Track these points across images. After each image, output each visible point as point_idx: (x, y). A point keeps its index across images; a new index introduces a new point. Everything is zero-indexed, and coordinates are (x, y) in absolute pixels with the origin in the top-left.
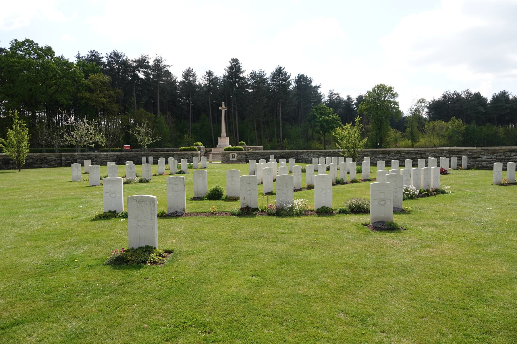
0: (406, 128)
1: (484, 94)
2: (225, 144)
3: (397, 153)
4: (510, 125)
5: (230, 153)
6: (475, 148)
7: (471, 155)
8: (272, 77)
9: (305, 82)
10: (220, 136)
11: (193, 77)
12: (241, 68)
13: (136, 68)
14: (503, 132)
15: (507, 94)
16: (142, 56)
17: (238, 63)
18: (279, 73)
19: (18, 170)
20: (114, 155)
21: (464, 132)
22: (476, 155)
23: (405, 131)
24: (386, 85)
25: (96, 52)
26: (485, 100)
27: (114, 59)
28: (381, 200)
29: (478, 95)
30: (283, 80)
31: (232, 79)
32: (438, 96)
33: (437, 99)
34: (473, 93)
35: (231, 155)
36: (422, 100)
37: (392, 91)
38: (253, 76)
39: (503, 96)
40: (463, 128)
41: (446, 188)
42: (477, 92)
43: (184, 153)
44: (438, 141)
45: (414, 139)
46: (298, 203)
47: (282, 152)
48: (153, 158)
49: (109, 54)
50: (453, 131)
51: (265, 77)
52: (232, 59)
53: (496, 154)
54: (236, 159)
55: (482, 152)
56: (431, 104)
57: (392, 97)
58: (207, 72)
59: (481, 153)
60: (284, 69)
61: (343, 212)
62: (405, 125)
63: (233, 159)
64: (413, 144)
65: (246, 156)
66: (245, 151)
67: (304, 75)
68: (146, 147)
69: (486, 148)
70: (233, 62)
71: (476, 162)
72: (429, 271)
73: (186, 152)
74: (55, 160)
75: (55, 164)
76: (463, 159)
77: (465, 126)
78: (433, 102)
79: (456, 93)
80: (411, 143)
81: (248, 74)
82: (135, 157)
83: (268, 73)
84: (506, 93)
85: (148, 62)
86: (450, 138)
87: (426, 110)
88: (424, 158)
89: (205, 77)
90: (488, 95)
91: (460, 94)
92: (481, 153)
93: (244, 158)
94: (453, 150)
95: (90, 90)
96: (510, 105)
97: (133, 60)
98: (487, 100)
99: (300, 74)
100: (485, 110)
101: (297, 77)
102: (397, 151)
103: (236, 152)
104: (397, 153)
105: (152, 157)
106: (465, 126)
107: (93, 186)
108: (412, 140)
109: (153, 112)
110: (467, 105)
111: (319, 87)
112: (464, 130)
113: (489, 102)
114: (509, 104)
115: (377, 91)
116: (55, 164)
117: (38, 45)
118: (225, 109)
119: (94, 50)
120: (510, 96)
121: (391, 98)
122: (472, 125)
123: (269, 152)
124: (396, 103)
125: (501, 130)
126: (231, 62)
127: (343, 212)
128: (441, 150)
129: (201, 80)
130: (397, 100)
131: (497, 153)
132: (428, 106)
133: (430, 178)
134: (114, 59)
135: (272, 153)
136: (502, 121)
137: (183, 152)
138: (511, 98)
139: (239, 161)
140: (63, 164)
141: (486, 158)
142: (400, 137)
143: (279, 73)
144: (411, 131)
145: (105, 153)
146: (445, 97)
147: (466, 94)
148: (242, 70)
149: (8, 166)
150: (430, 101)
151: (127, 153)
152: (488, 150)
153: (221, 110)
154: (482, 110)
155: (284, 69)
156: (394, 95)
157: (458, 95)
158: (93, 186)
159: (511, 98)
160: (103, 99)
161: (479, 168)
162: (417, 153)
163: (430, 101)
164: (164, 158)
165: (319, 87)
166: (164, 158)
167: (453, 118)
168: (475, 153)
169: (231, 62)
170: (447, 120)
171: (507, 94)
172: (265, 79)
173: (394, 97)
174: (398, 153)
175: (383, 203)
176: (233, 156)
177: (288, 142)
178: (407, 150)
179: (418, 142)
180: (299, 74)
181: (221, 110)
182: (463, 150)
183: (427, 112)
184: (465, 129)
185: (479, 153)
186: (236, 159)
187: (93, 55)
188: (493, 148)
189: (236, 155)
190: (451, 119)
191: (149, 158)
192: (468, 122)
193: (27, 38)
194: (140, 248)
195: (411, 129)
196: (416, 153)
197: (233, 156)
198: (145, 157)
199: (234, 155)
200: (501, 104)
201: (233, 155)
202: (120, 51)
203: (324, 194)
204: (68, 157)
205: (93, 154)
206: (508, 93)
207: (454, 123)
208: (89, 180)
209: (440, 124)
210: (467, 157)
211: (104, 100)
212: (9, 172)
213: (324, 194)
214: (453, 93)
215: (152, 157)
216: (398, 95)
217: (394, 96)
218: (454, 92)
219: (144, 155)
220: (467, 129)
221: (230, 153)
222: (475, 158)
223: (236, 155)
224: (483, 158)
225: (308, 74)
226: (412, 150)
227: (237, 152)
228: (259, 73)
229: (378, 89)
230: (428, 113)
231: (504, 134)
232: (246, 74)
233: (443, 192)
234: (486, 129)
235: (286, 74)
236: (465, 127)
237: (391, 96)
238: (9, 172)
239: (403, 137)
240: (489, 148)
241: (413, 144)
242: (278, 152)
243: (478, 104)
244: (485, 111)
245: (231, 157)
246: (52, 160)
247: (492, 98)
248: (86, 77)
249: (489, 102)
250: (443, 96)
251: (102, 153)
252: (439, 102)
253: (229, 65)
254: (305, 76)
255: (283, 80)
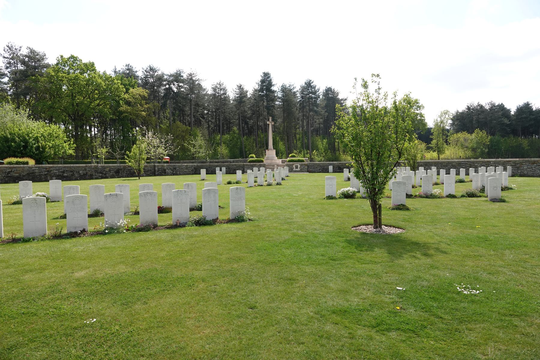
0: (432, 139)
1: (507, 106)
2: (272, 156)
3: (448, 164)
4: (534, 137)
5: (293, 164)
6: (518, 159)
7: (515, 166)
8: (301, 90)
9: (332, 95)
10: (267, 148)
11: (224, 90)
12: (272, 81)
13: (172, 82)
14: (527, 143)
15: (530, 105)
16: (177, 71)
17: (269, 77)
18: (309, 85)
19: (138, 178)
20: (192, 166)
21: (488, 143)
22: (518, 165)
23: (431, 143)
24: (412, 97)
25: (131, 66)
26: (509, 111)
27: (149, 73)
28: (494, 187)
29: (501, 107)
30: (312, 93)
31: (263, 93)
32: (462, 108)
33: (460, 111)
34: (497, 104)
35: (294, 166)
36: (445, 112)
37: (418, 103)
38: (284, 89)
39: (526, 107)
40: (488, 140)
41: (513, 186)
42: (500, 104)
43: (253, 165)
44: (463, 152)
45: (440, 151)
46: (436, 191)
47: (340, 164)
48: (226, 169)
49: (145, 69)
50: (477, 143)
51: (295, 90)
52: (263, 73)
53: (535, 165)
54: (299, 169)
55: (524, 162)
56: (454, 115)
57: (418, 109)
58: (237, 86)
59: (523, 164)
60: (313, 82)
61: (463, 196)
62: (431, 137)
63: (297, 169)
64: (439, 156)
65: (308, 167)
66: (307, 163)
67: (332, 88)
68: (208, 159)
69: (527, 159)
70: (264, 76)
71: (519, 171)
72: (433, 298)
73: (254, 163)
74: (150, 170)
75: (150, 174)
76: (508, 168)
77: (489, 137)
78: (457, 113)
79: (479, 105)
80: (437, 155)
81: (279, 88)
82: (209, 168)
83: (297, 85)
84: (530, 104)
85: (182, 77)
86: (474, 150)
87: (450, 122)
88: (455, 169)
89: (236, 90)
90: (512, 107)
91: (484, 105)
92: (523, 164)
93: (306, 168)
94: (499, 161)
95: (128, 103)
96: (534, 117)
97: (168, 75)
98: (511, 111)
99: (328, 87)
100: (509, 121)
101: (324, 90)
102: (449, 162)
103: (299, 163)
104: (448, 164)
105: (225, 168)
106: (489, 137)
107: (250, 187)
108: (438, 152)
109: (488, 148)
110: (491, 117)
111: (346, 100)
112: (489, 142)
113: (512, 113)
114: (533, 115)
115: (403, 103)
116: (150, 174)
117: (81, 61)
118: (272, 124)
119: (129, 64)
120: (533, 107)
121: (417, 110)
122: (497, 137)
123: (328, 163)
124: (422, 116)
125: (524, 142)
126: (262, 76)
127: (463, 196)
128: (488, 161)
129: (232, 94)
130: (423, 112)
131: (536, 164)
132: (452, 117)
133: (502, 179)
134: (149, 73)
135: (331, 164)
136: (527, 132)
137: (252, 163)
138: (534, 109)
139: (301, 171)
140: (157, 173)
141: (527, 168)
142: (425, 148)
143: (309, 85)
144: (437, 143)
145: (186, 164)
146: (469, 108)
147: (490, 105)
148: (273, 83)
149: (118, 175)
150: (454, 113)
151: (203, 164)
152: (529, 161)
153: (269, 124)
154: (506, 121)
155: (313, 82)
156: (420, 106)
157: (482, 107)
158: (250, 187)
159: (534, 109)
160: (143, 113)
161: (521, 176)
162: (467, 164)
163: (454, 113)
164: (205, 169)
165: (346, 100)
166: (205, 169)
167: (477, 129)
168: (518, 163)
169: (262, 76)
170: (471, 132)
171: (530, 105)
172: (295, 93)
173: (420, 110)
174: (450, 164)
175: (495, 189)
176: (297, 167)
177: (317, 155)
178: (457, 162)
179: (444, 153)
180: (326, 87)
181: (269, 124)
182: (507, 161)
183: (451, 124)
184: (489, 140)
185: (521, 163)
186: (299, 169)
187: (128, 69)
188: (533, 159)
189: (299, 166)
190: (475, 130)
191: (223, 168)
192: (493, 134)
193: (72, 54)
194: (402, 204)
195: (437, 141)
196: (465, 164)
197: (297, 167)
198: (219, 168)
199: (297, 166)
200: (525, 116)
201: (296, 166)
202: (155, 66)
203: (450, 186)
204: (160, 167)
205: (177, 165)
206: (531, 104)
207: (478, 135)
208: (247, 182)
209: (462, 136)
210: (511, 167)
211: (144, 113)
212: (131, 180)
213: (450, 186)
214: (477, 104)
215: (225, 168)
216: (424, 107)
217: (420, 108)
218: (478, 103)
219: (217, 166)
220: (491, 141)
221: (293, 164)
222: (518, 168)
223: (299, 166)
224: (525, 168)
225: (336, 87)
226: (462, 161)
227: (300, 163)
228: (289, 86)
229: (404, 102)
230: (452, 125)
231: (528, 146)
232: (277, 88)
233: (511, 189)
234: (512, 141)
235: (315, 87)
236: (489, 138)
237: (417, 108)
238: (131, 180)
239: (428, 148)
240: (529, 159)
241: (439, 156)
242: (336, 164)
243: (502, 115)
244: (509, 123)
245: (295, 168)
246: (148, 170)
247: (516, 110)
248: (127, 92)
249: (512, 113)
250: (467, 107)
251: (183, 164)
252: (463, 113)
253: (260, 78)
254: (333, 89)
255: (312, 93)
